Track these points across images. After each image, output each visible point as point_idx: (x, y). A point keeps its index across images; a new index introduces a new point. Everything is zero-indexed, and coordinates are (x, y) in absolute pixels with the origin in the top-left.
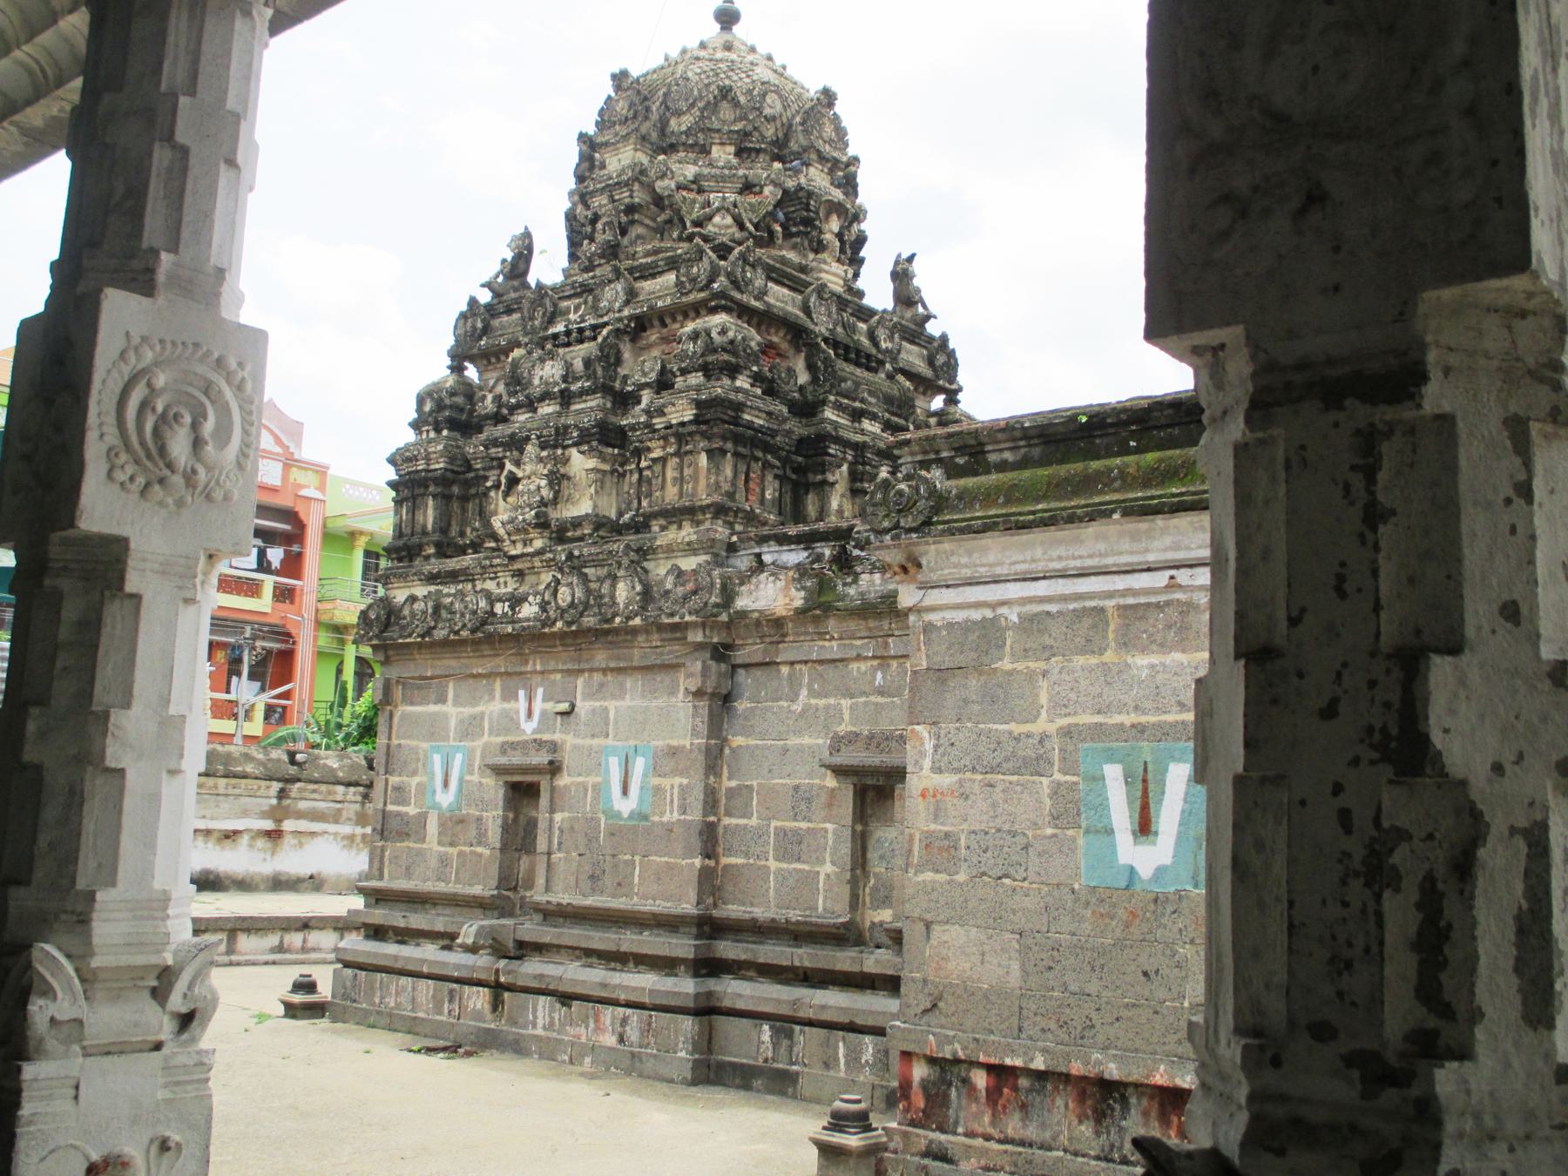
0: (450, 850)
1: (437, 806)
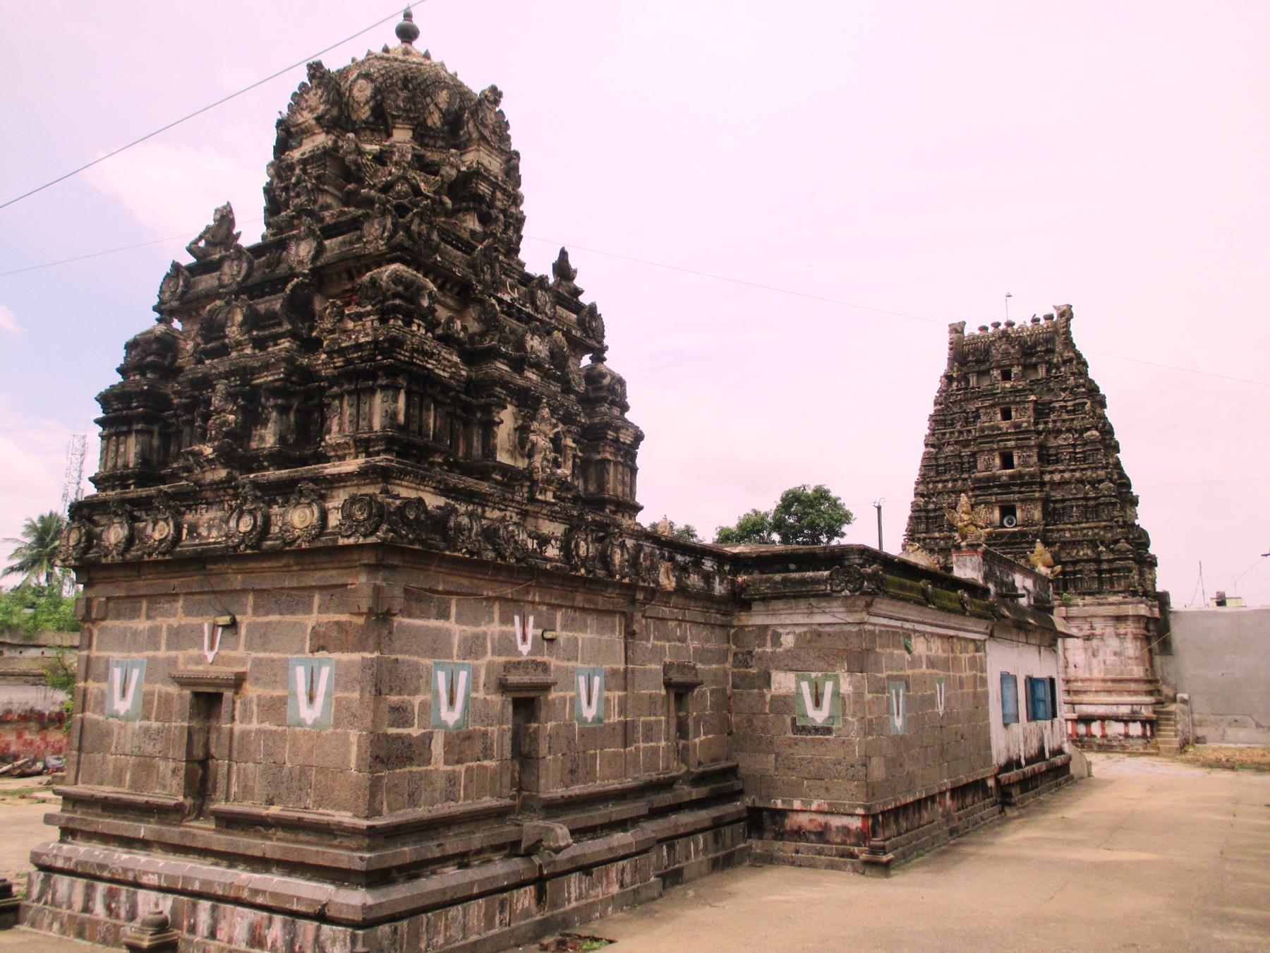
0: (458, 767)
1: (443, 725)
